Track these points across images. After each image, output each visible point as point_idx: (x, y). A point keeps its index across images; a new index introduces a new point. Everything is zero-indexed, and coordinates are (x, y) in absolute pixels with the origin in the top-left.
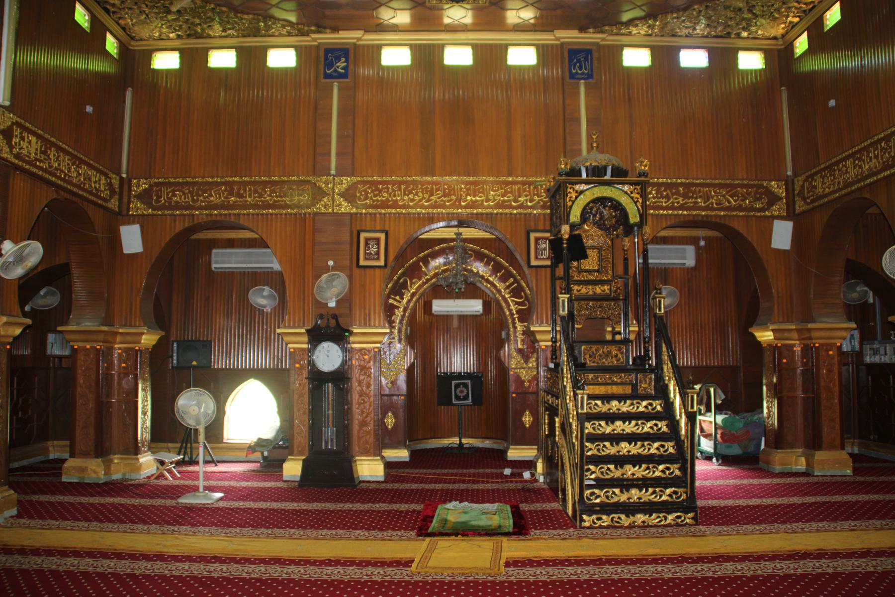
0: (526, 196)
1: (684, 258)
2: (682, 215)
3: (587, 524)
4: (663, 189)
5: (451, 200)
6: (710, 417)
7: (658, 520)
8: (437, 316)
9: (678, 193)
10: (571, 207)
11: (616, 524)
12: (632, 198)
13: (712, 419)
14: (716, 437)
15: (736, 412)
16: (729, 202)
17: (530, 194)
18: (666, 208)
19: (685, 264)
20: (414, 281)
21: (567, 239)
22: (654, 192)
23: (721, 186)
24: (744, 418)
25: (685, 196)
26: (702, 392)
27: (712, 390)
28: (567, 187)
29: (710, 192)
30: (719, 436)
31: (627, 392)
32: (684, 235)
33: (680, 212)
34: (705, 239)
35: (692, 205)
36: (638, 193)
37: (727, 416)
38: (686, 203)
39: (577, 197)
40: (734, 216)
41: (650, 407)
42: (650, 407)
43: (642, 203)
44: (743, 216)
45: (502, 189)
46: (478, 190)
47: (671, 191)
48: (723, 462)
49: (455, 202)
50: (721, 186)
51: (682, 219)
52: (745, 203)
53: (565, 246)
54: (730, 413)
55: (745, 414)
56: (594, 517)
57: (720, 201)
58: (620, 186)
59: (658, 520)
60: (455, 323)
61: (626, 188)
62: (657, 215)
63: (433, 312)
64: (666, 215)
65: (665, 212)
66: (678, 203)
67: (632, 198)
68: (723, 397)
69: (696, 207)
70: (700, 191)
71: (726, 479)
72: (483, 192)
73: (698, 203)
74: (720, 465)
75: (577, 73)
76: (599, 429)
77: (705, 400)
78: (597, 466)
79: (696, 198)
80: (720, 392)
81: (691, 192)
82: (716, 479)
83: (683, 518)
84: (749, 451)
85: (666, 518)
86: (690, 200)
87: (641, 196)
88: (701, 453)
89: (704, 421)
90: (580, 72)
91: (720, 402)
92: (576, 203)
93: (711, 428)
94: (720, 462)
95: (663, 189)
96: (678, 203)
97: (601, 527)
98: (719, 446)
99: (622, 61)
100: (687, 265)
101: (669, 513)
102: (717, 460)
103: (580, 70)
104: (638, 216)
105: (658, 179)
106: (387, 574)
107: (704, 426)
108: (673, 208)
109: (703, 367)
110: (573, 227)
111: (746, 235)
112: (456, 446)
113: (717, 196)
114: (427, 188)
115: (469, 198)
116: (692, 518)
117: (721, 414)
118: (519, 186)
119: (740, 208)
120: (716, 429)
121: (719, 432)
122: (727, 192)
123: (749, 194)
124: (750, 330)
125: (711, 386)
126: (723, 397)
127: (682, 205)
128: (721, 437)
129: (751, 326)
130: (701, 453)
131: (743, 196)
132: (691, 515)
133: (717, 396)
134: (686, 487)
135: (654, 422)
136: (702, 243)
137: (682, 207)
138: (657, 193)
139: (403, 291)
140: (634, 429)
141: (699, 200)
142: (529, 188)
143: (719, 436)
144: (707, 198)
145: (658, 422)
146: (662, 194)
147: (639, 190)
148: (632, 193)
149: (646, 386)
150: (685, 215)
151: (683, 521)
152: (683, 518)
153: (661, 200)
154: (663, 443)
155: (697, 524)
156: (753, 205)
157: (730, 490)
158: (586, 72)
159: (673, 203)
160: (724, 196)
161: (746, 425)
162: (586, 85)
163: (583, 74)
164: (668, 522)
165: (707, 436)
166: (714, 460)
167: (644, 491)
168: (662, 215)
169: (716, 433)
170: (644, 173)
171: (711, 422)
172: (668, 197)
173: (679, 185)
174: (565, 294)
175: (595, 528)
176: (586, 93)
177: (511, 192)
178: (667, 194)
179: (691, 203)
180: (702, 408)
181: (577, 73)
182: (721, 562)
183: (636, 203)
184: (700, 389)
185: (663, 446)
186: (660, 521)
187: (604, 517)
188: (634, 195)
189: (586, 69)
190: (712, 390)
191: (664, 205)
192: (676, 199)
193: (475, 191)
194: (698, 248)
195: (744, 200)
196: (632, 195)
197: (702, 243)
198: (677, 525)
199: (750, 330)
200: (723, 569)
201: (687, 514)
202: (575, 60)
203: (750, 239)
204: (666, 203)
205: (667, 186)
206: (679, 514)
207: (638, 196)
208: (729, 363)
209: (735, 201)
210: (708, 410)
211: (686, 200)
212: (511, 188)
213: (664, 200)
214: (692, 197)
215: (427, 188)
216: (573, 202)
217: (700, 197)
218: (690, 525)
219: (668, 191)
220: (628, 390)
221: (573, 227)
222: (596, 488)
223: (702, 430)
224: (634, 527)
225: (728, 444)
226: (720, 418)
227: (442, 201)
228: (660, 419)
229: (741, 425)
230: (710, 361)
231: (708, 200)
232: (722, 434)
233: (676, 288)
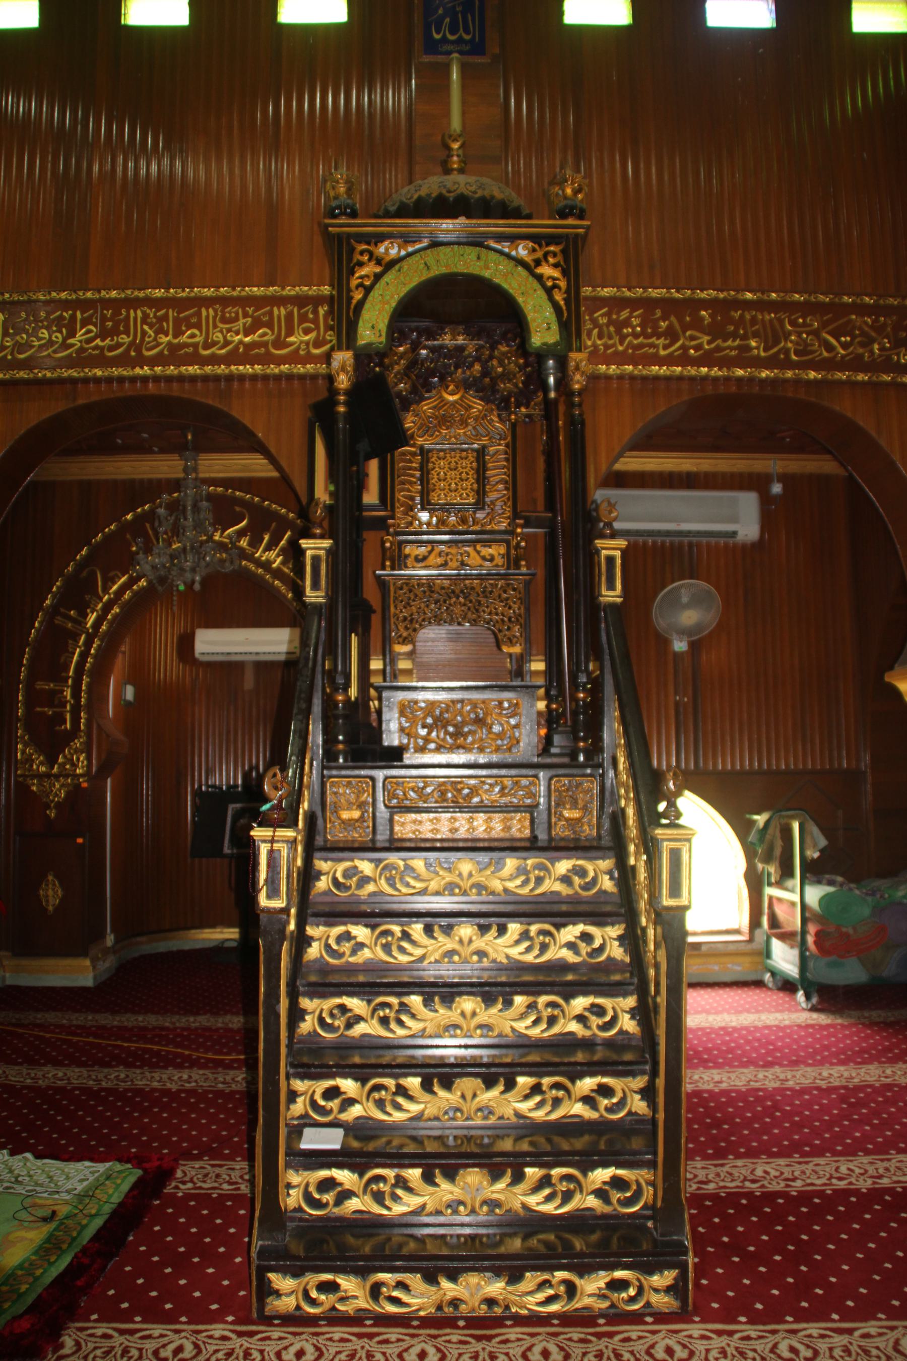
0: (307, 332)
1: (734, 519)
2: (705, 378)
3: (287, 1304)
4: (658, 313)
5: (119, 345)
6: (792, 891)
7: (541, 1296)
8: (209, 665)
9: (697, 324)
10: (361, 304)
11: (392, 1309)
12: (539, 278)
13: (796, 898)
14: (803, 942)
15: (854, 876)
16: (830, 348)
17: (317, 328)
18: (669, 361)
19: (734, 534)
20: (111, 574)
21: (347, 393)
22: (635, 321)
23: (808, 309)
24: (873, 893)
25: (716, 332)
26: (770, 831)
27: (796, 826)
28: (352, 250)
29: (781, 322)
30: (810, 939)
31: (515, 832)
32: (734, 469)
33: (704, 370)
34: (784, 478)
35: (733, 353)
36: (556, 266)
37: (831, 889)
38: (718, 349)
39: (378, 277)
40: (840, 382)
41: (577, 880)
42: (577, 880)
43: (568, 291)
44: (863, 383)
45: (246, 315)
46: (187, 319)
47: (681, 321)
48: (822, 1000)
49: (127, 351)
50: (808, 309)
51: (709, 390)
52: (872, 352)
53: (342, 409)
54: (840, 879)
55: (876, 883)
56: (313, 1279)
57: (806, 345)
58: (505, 247)
59: (541, 1296)
60: (249, 682)
61: (522, 251)
62: (644, 379)
63: (197, 655)
64: (668, 379)
65: (664, 370)
66: (697, 348)
67: (539, 278)
68: (823, 842)
69: (744, 359)
70: (754, 321)
71: (821, 1063)
72: (198, 326)
73: (749, 348)
74: (813, 1009)
75: (444, 40)
76: (402, 950)
77: (778, 851)
78: (363, 1080)
79: (745, 337)
80: (815, 830)
81: (731, 321)
82: (795, 1063)
83: (632, 1292)
84: (885, 974)
85: (571, 1289)
86: (730, 343)
87: (565, 273)
88: (773, 974)
89: (780, 900)
90: (451, 38)
91: (816, 855)
92: (375, 294)
93: (794, 916)
94: (815, 1000)
95: (658, 313)
96: (697, 348)
97: (335, 1319)
98: (811, 964)
99: (561, 13)
100: (740, 537)
101: (583, 1270)
102: (808, 997)
103: (452, 33)
104: (555, 327)
105: (645, 288)
106: (187, 1179)
107: (780, 911)
108: (684, 360)
109: (778, 772)
110: (364, 357)
111: (874, 434)
112: (234, 944)
113: (799, 335)
114: (61, 317)
115: (164, 339)
116: (668, 1290)
117: (819, 882)
118: (290, 307)
119: (856, 364)
120: (804, 921)
121: (812, 928)
122: (824, 325)
123: (880, 329)
124: (887, 678)
125: (793, 817)
126: (823, 842)
127: (708, 353)
128: (815, 942)
129: (891, 668)
130: (773, 974)
131: (863, 334)
132: (663, 1279)
133: (808, 840)
134: (653, 1165)
135: (580, 928)
136: (777, 488)
137: (707, 359)
138: (643, 325)
139: (87, 597)
140: (516, 952)
141: (753, 344)
142: (315, 312)
143: (810, 939)
144: (773, 337)
145: (591, 929)
146: (656, 327)
147: (560, 258)
148: (538, 263)
149: (576, 814)
150: (716, 379)
151: (632, 1300)
152: (632, 1292)
153: (653, 340)
154: (600, 1001)
155: (681, 1316)
156: (889, 358)
157: (825, 1109)
158: (467, 37)
159: (684, 348)
160: (816, 333)
161: (878, 911)
162: (464, 70)
163: (460, 41)
164: (577, 1304)
165: (785, 937)
166: (800, 995)
167: (507, 1179)
168: (657, 378)
169: (804, 932)
170: (572, 208)
171: (793, 904)
172: (672, 335)
173: (697, 305)
174: (322, 537)
175: (312, 1321)
176: (464, 87)
177: (270, 325)
178: (670, 327)
179: (731, 348)
180: (772, 869)
181: (444, 40)
182: (860, 1063)
183: (549, 291)
184: (767, 823)
185: (599, 1011)
186: (550, 1300)
187: (347, 1283)
188: (546, 270)
189: (467, 31)
190: (796, 826)
191: (662, 353)
192: (692, 338)
193: (178, 322)
194: (766, 500)
195: (867, 343)
196: (539, 270)
197: (777, 488)
198: (617, 1317)
199: (887, 678)
200: (862, 1074)
201: (651, 1273)
202: (440, 11)
203: (882, 442)
204: (665, 347)
205: (669, 306)
206: (619, 1274)
207: (556, 273)
208: (840, 764)
209: (845, 346)
210: (786, 871)
211: (719, 342)
212: (271, 313)
213: (661, 341)
214: (735, 335)
215: (61, 317)
216: (368, 290)
217: (755, 335)
218: (661, 1318)
219: (673, 318)
220: (519, 827)
221: (364, 357)
222: (340, 1166)
223: (774, 922)
224: (450, 1322)
225: (833, 958)
226: (814, 894)
227: (97, 347)
228: (599, 917)
229: (866, 911)
230: (796, 758)
231: (776, 342)
232: (818, 934)
233: (717, 588)
